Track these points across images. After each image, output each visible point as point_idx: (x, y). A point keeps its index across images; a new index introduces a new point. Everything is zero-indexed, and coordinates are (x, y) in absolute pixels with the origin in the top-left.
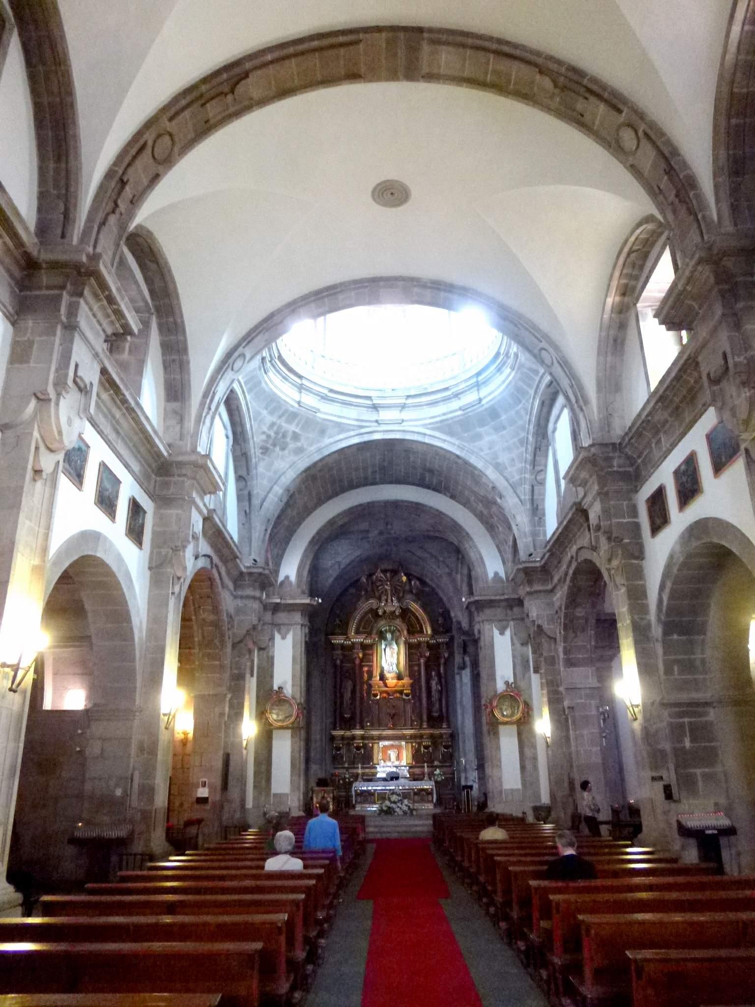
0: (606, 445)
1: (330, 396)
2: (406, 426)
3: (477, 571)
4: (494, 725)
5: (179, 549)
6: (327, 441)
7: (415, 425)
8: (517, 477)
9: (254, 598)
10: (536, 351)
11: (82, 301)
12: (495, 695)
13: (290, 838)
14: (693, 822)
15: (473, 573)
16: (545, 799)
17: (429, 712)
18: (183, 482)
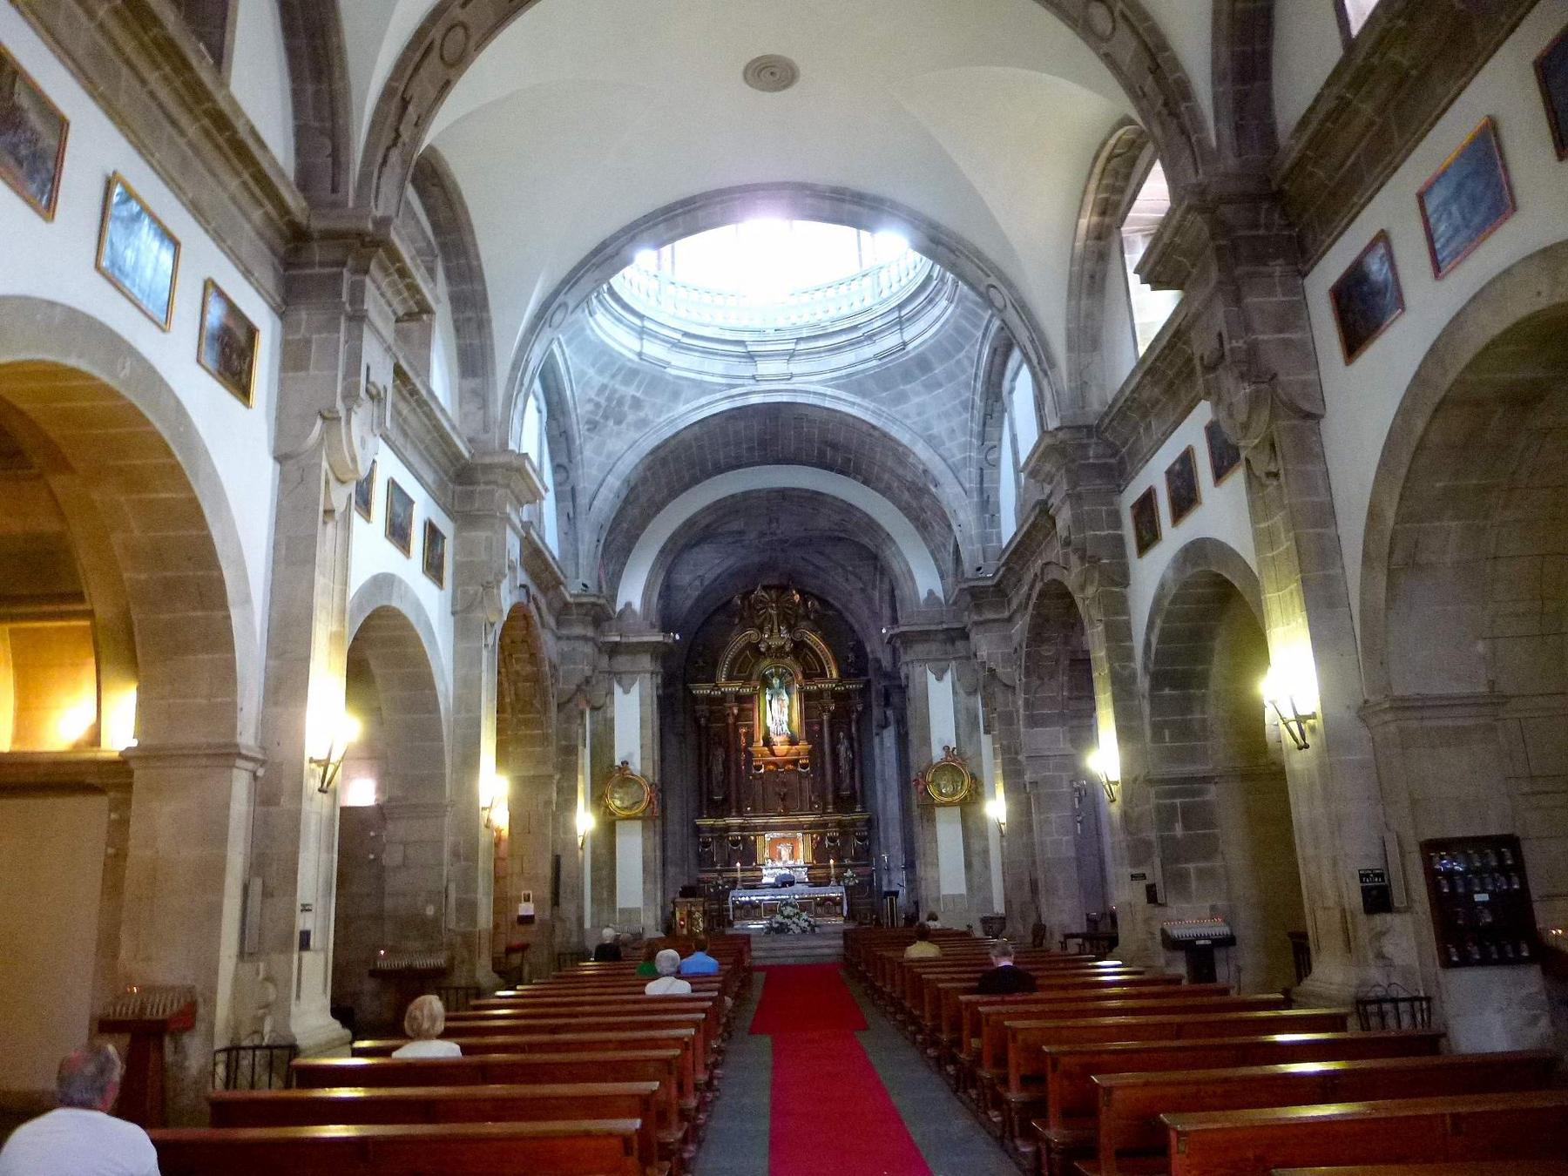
0: (1079, 428)
1: (685, 342)
2: (796, 384)
3: (903, 591)
4: (929, 807)
5: (489, 587)
6: (682, 408)
7: (810, 382)
8: (959, 456)
9: (585, 638)
10: (982, 289)
11: (368, 281)
12: (930, 765)
13: (673, 959)
14: (1178, 931)
15: (897, 592)
16: (999, 908)
17: (837, 790)
18: (492, 493)
